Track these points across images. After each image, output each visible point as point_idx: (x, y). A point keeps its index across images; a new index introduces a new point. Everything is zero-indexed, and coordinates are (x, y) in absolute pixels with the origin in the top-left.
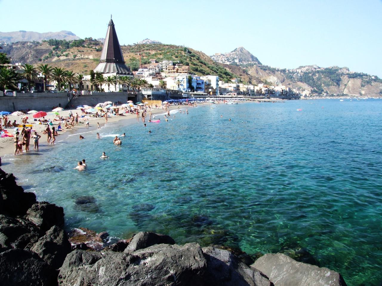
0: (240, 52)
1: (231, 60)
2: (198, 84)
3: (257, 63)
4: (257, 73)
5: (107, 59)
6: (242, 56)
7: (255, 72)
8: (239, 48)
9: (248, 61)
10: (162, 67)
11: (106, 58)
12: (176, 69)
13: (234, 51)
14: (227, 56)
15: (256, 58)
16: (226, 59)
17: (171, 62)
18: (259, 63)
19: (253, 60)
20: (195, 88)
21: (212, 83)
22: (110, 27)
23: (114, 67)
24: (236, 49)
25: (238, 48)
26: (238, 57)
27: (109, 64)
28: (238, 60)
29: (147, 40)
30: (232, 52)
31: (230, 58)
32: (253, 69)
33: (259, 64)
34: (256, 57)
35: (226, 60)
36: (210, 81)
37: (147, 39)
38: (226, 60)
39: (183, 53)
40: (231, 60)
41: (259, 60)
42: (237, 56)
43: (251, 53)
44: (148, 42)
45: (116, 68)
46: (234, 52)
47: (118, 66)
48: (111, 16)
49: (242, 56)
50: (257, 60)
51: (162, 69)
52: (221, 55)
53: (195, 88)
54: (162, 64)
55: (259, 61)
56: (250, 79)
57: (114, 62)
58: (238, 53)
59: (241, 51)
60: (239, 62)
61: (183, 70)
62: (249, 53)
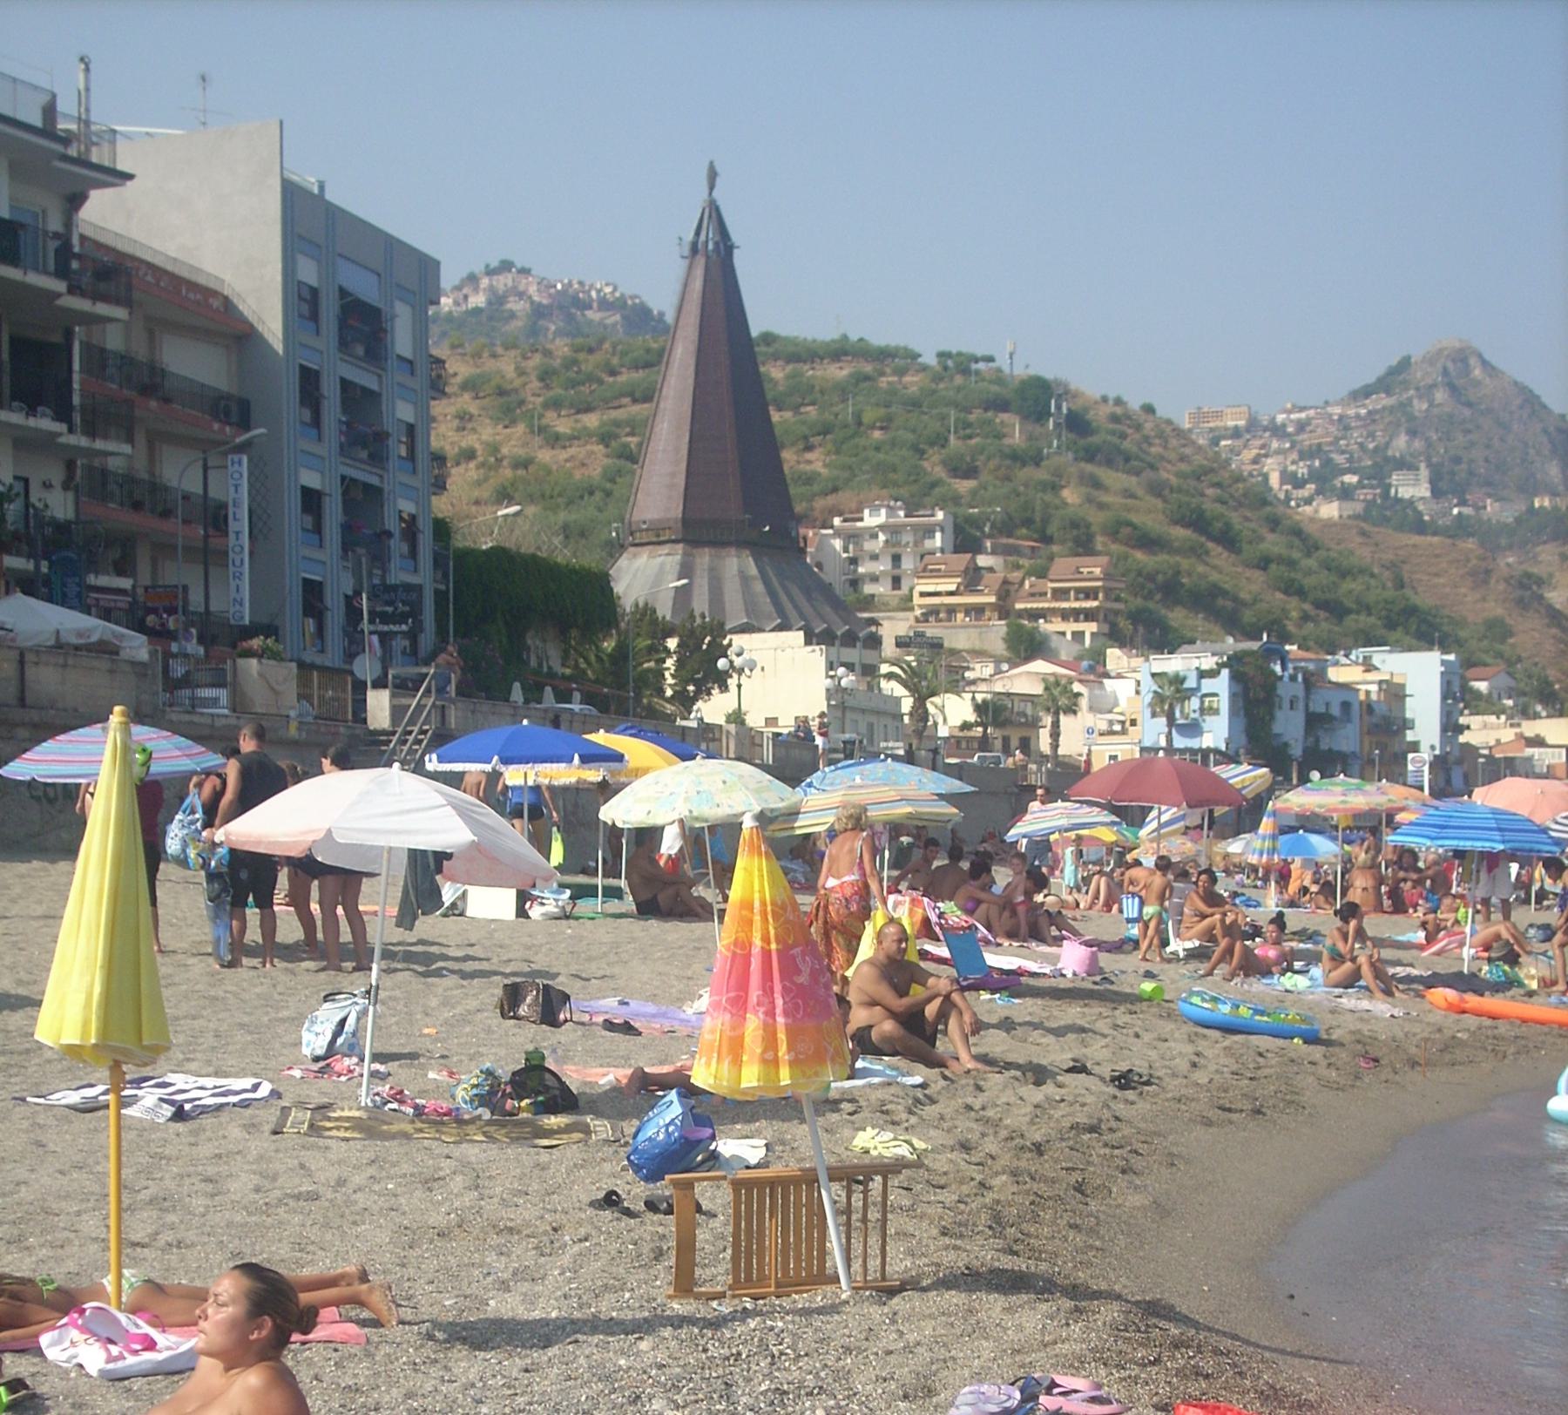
0: (1440, 396)
2: (1315, 721)
5: (686, 521)
6: (1460, 439)
8: (1431, 360)
9: (1530, 487)
10: (854, 561)
11: (677, 512)
12: (993, 580)
13: (1385, 384)
14: (1306, 440)
16: (1302, 470)
17: (940, 515)
20: (1297, 751)
21: (1412, 709)
22: (701, 262)
23: (745, 579)
24: (1405, 363)
25: (1417, 355)
26: (1418, 444)
27: (704, 558)
29: (503, 281)
30: (1366, 392)
31: (1339, 459)
35: (1299, 483)
36: (1395, 692)
37: (506, 266)
38: (1299, 483)
39: (1016, 432)
42: (1413, 433)
44: (521, 295)
45: (759, 587)
46: (1380, 401)
47: (769, 571)
49: (1460, 439)
51: (855, 583)
53: (1297, 751)
57: (741, 544)
58: (1420, 406)
59: (1453, 389)
60: (1437, 493)
61: (1060, 594)
62: (1531, 402)
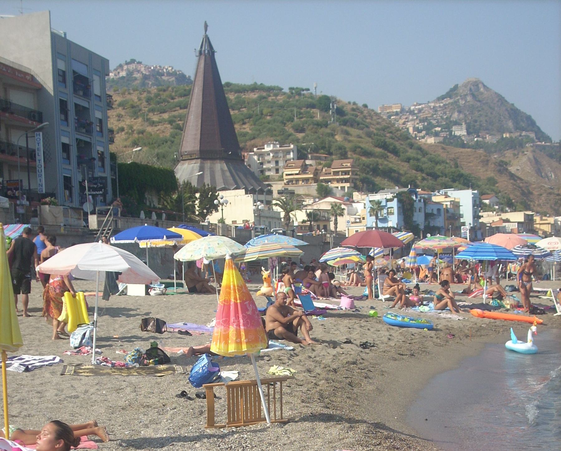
0: (469, 98)
1: (438, 129)
2: (428, 216)
3: (532, 135)
4: (539, 171)
6: (477, 114)
7: (528, 168)
8: (465, 85)
9: (501, 130)
10: (262, 164)
13: (449, 95)
14: (422, 115)
15: (529, 118)
16: (420, 126)
17: (292, 146)
18: (541, 136)
19: (518, 128)
21: (462, 210)
23: (223, 171)
24: (456, 87)
27: (208, 164)
28: (464, 126)
29: (132, 67)
30: (442, 98)
31: (434, 122)
32: (525, 159)
33: (539, 139)
34: (528, 113)
35: (420, 131)
36: (456, 205)
37: (133, 61)
38: (420, 131)
39: (318, 116)
40: (438, 129)
41: (538, 124)
42: (460, 112)
43: (510, 99)
45: (228, 174)
46: (448, 101)
47: (232, 168)
48: (206, 26)
50: (531, 124)
51: (262, 171)
52: (402, 110)
54: (261, 155)
55: (539, 128)
56: (523, 194)
57: (221, 159)
58: (462, 102)
60: (469, 133)
61: (336, 173)
62: (502, 100)
